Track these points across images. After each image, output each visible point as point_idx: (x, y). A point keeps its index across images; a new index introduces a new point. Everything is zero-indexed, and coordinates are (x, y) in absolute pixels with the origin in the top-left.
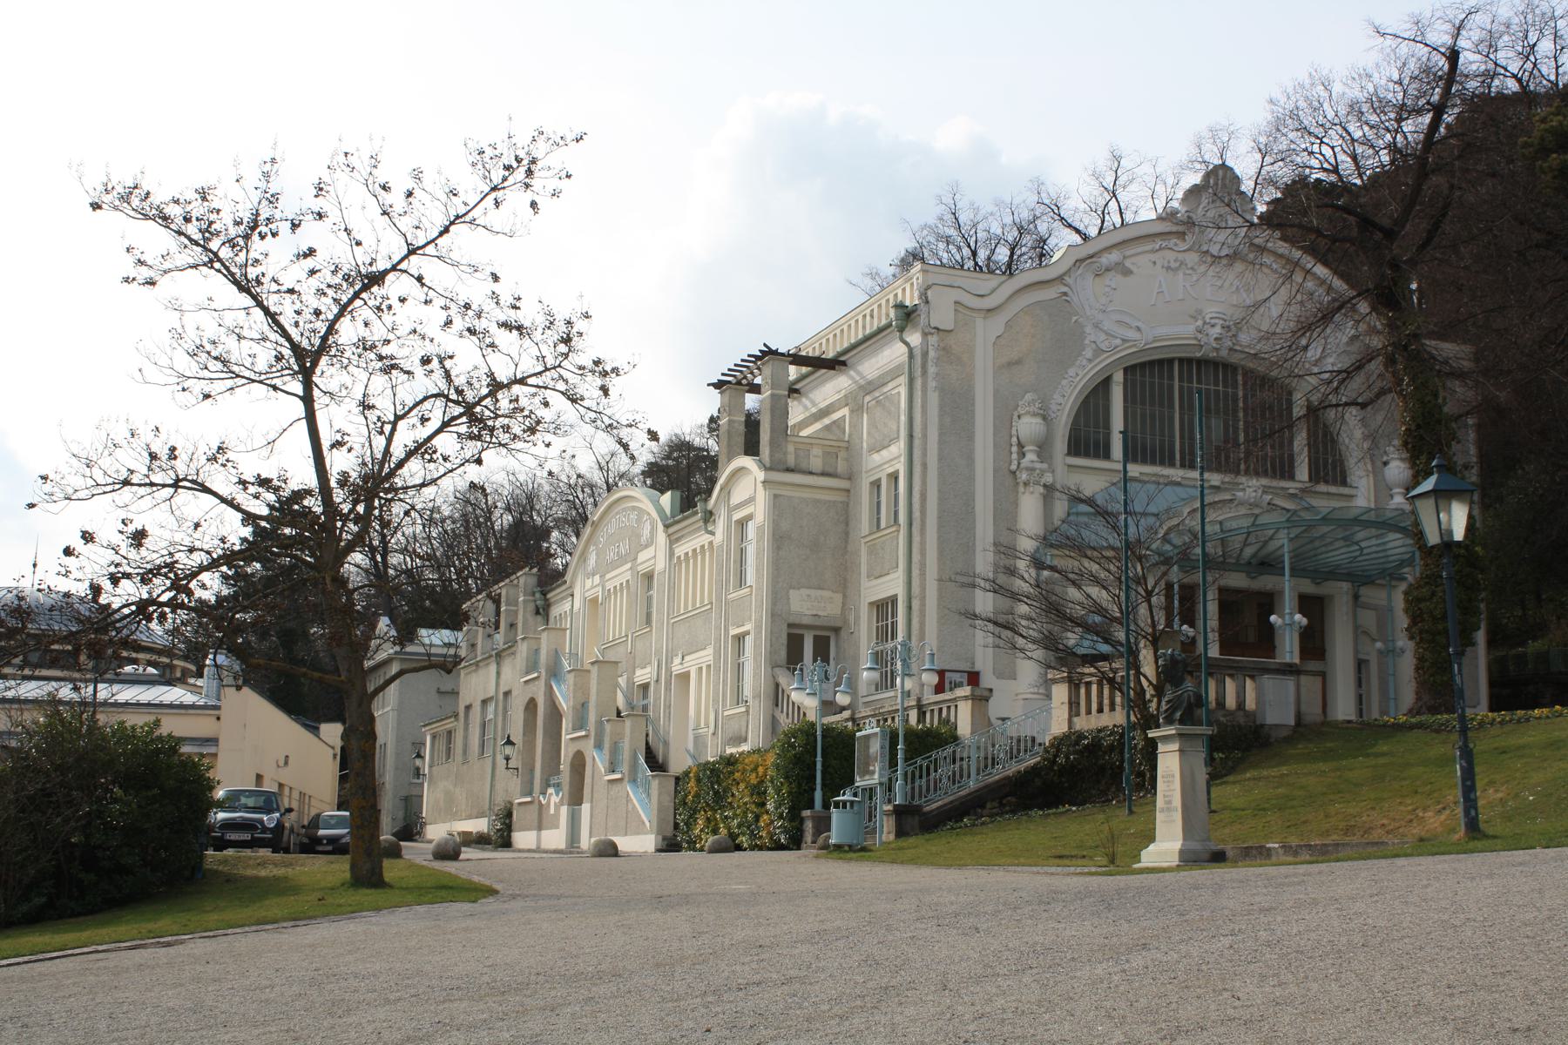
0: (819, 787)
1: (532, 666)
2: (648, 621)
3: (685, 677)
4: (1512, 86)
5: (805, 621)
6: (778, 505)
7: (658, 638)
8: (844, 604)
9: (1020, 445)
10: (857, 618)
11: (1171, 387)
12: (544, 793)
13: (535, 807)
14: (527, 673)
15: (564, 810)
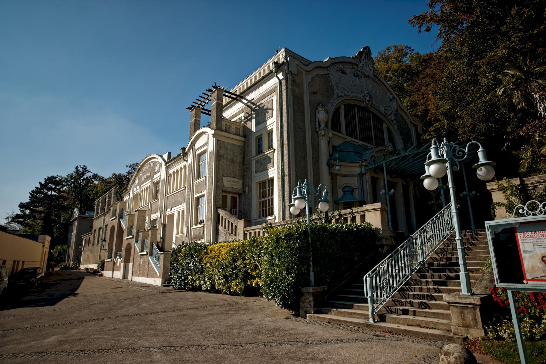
1: (114, 215)
2: (156, 197)
3: (172, 216)
4: (88, 265)
5: (229, 190)
6: (219, 144)
7: (160, 202)
8: (243, 184)
9: (319, 123)
10: (250, 189)
12: (115, 258)
13: (112, 262)
14: (112, 217)
15: (122, 265)
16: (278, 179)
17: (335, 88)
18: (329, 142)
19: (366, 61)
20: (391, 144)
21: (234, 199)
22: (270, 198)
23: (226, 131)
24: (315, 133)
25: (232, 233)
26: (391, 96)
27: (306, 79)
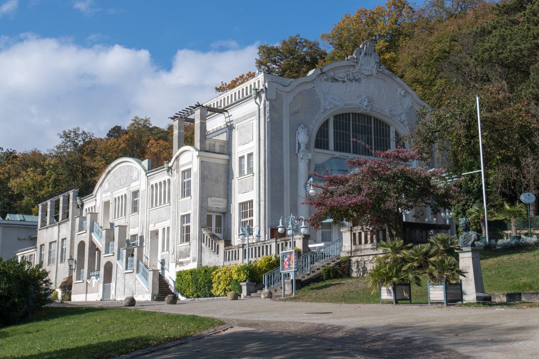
5: (214, 210)
11: (349, 123)
17: (322, 101)
21: (218, 218)
22: (251, 218)
24: (294, 156)
26: (403, 92)
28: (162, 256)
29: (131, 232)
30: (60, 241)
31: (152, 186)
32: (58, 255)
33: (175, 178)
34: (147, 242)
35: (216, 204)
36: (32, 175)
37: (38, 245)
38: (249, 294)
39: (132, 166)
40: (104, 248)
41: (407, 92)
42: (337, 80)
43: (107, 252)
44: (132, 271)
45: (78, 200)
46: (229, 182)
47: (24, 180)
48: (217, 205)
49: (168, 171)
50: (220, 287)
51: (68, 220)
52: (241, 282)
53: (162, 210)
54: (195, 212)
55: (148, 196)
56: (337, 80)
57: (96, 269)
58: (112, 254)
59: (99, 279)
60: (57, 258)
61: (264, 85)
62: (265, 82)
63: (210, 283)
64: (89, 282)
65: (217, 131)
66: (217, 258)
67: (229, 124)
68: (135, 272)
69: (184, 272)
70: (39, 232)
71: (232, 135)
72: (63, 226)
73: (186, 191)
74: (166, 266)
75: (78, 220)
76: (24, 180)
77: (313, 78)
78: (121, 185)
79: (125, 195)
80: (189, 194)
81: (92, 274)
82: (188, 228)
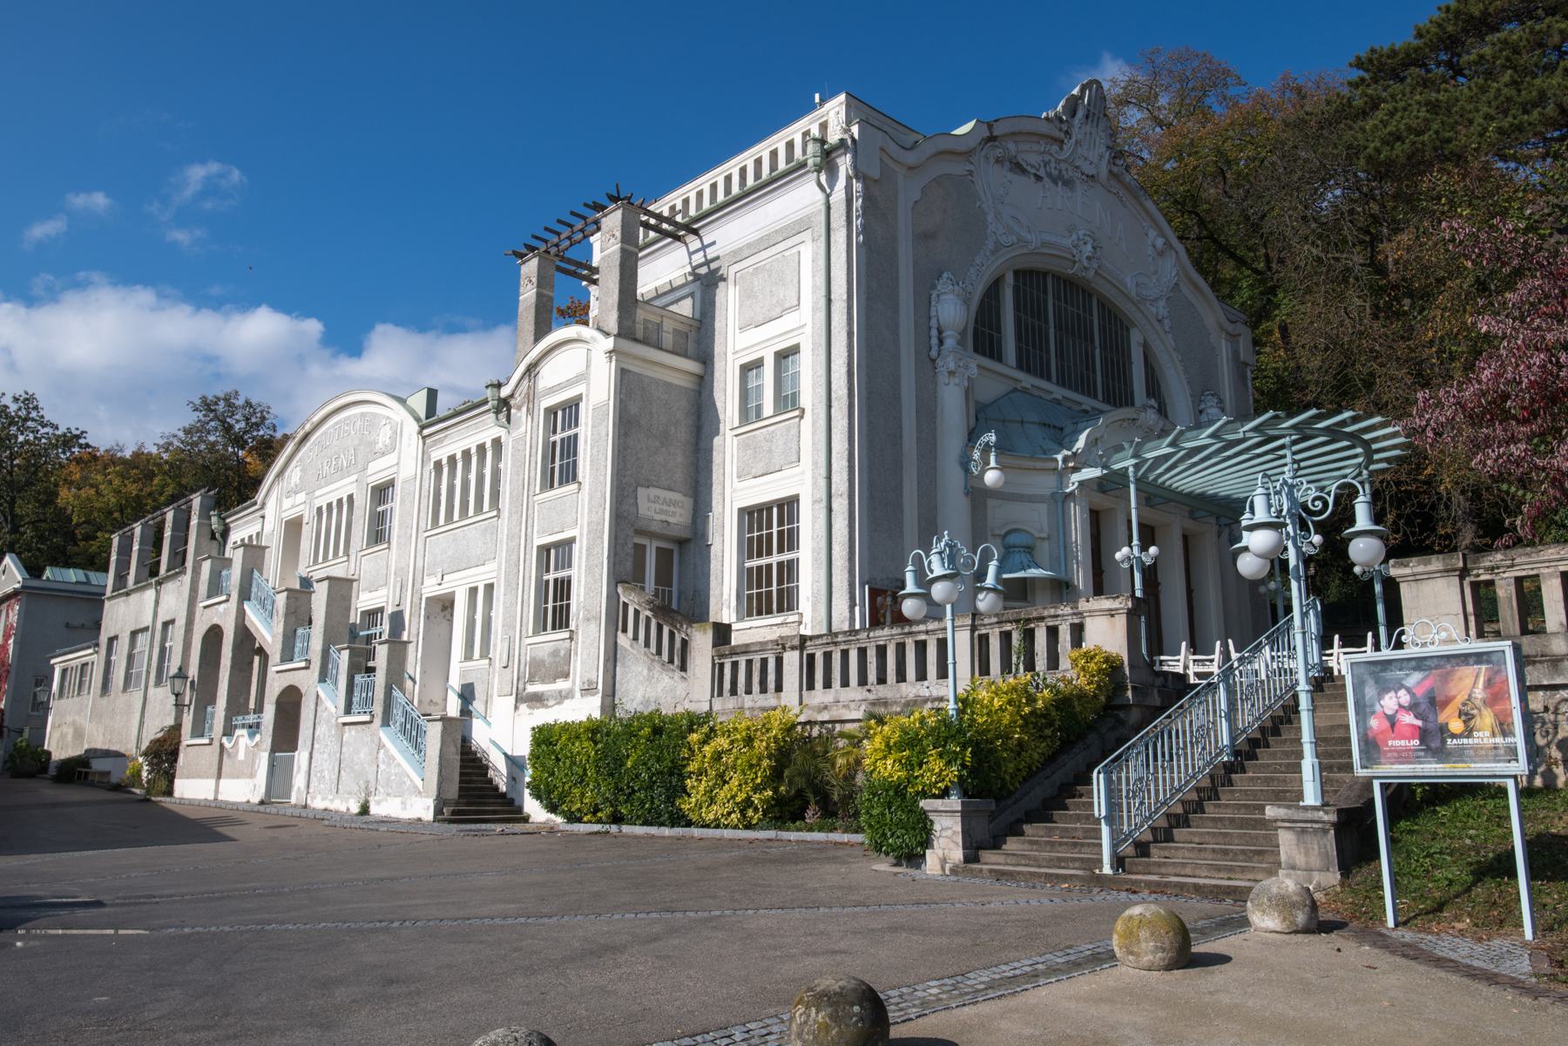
0: (1308, 749)
5: (654, 528)
6: (628, 385)
9: (940, 332)
16: (814, 502)
17: (990, 218)
18: (967, 392)
19: (1088, 128)
20: (1152, 402)
21: (664, 557)
22: (786, 557)
23: (645, 342)
24: (928, 363)
25: (671, 661)
26: (1160, 242)
27: (908, 192)
28: (463, 674)
29: (364, 601)
30: (159, 626)
31: (438, 465)
32: (149, 665)
33: (522, 429)
34: (414, 631)
35: (661, 512)
36: (117, 482)
37: (103, 639)
38: (972, 853)
39: (375, 415)
40: (279, 646)
41: (1168, 244)
42: (1024, 171)
43: (287, 655)
44: (367, 718)
45: (214, 519)
46: (702, 445)
47: (98, 493)
48: (666, 513)
49: (498, 412)
50: (722, 794)
51: (183, 572)
52: (924, 794)
53: (470, 534)
54: (594, 533)
55: (424, 493)
56: (1024, 171)
57: (252, 706)
58: (303, 664)
59: (258, 738)
60: (148, 672)
61: (847, 131)
62: (849, 122)
63: (673, 780)
64: (227, 745)
65: (673, 290)
66: (684, 685)
67: (704, 270)
68: (378, 721)
69: (566, 727)
70: (107, 604)
71: (712, 303)
72: (169, 587)
73: (560, 465)
74: (477, 706)
75: (206, 567)
76: (98, 493)
77: (972, 143)
78: (339, 469)
79: (350, 498)
80: (569, 475)
81: (239, 720)
82: (563, 588)
